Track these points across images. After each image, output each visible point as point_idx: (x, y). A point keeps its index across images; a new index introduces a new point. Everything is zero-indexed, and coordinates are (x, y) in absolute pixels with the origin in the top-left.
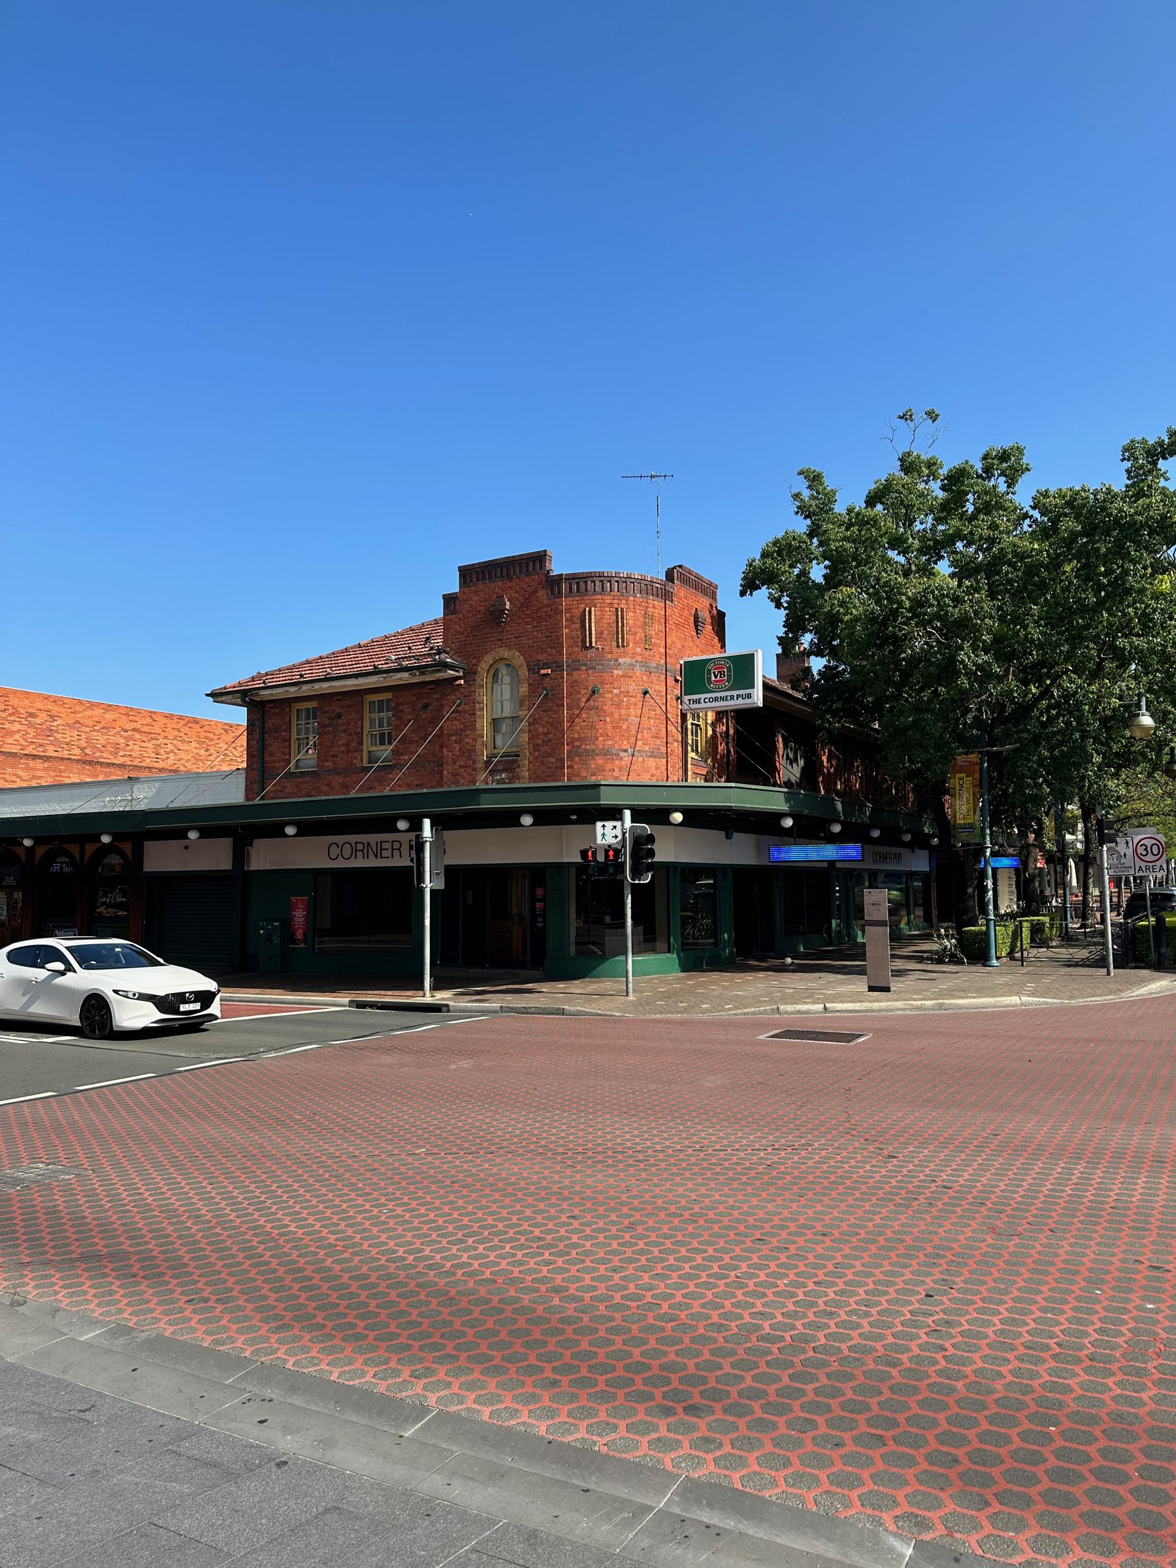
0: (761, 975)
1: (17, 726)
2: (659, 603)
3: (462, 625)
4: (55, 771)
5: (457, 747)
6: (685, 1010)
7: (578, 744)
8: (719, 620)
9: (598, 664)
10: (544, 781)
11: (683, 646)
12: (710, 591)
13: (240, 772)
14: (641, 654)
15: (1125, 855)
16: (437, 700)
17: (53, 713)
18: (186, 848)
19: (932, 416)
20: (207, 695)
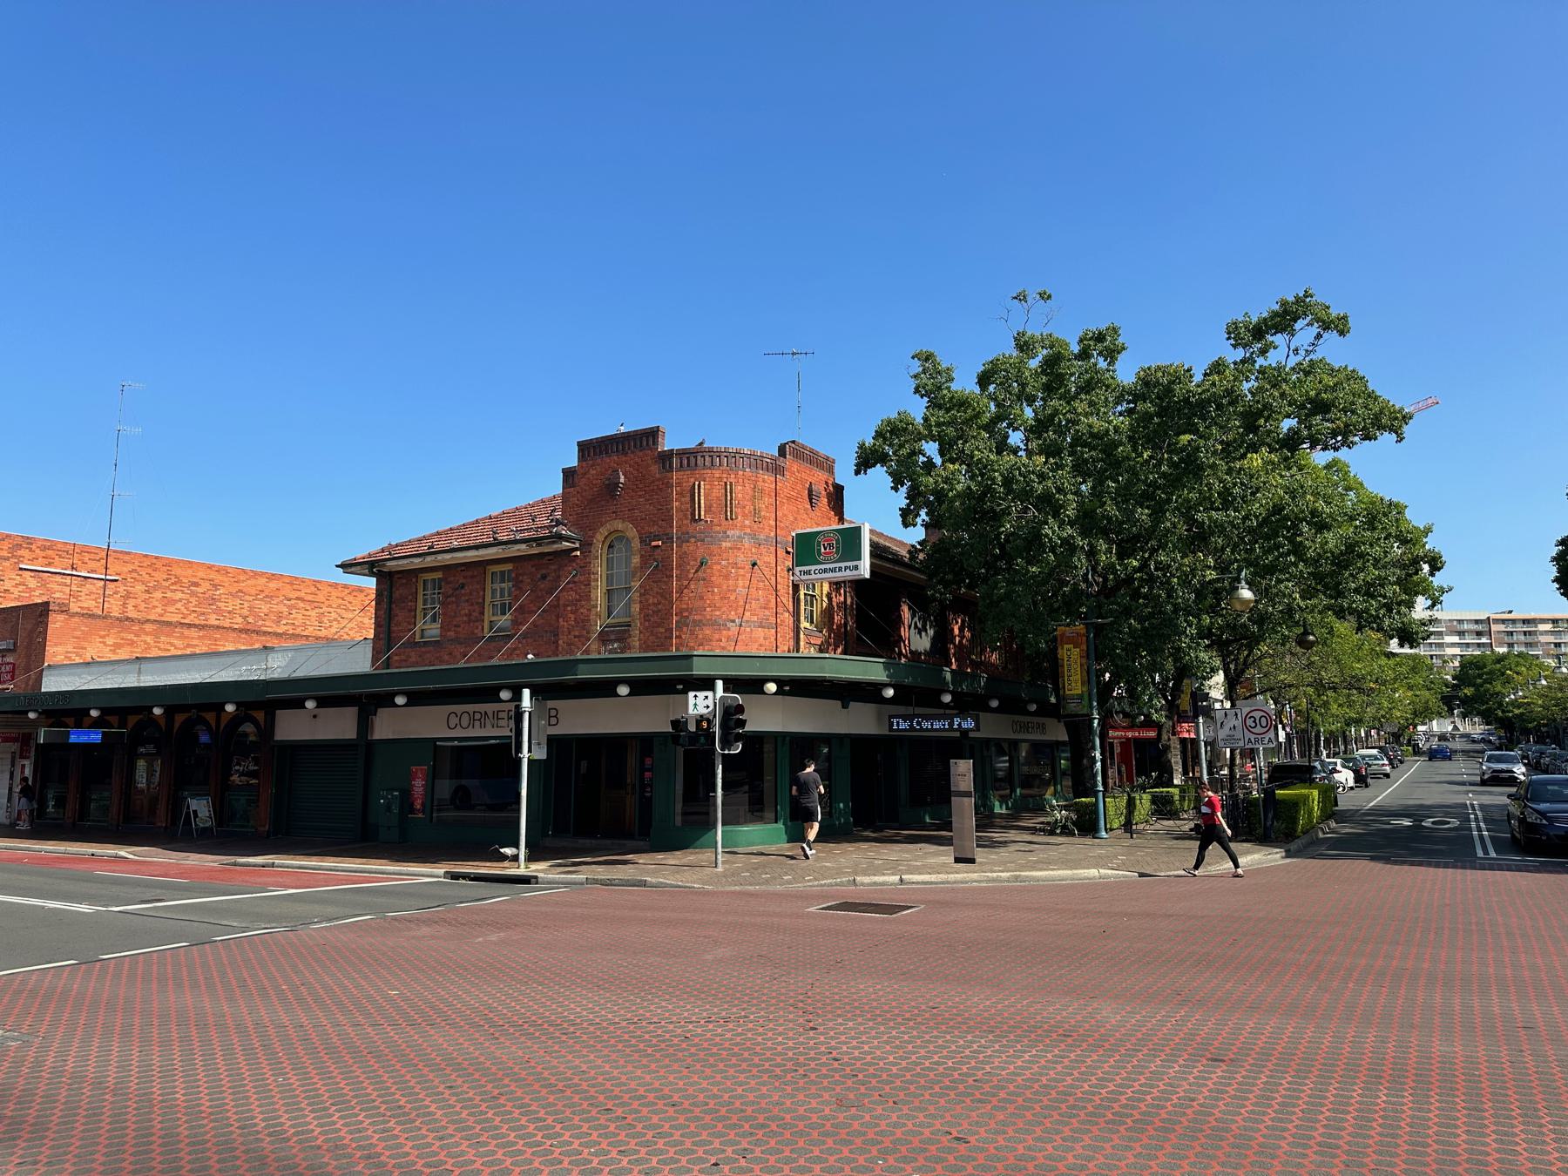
0: (865, 846)
1: (179, 595)
2: (769, 477)
5: (573, 616)
6: (767, 882)
7: (686, 614)
8: (836, 497)
10: (655, 651)
11: (796, 519)
12: (827, 465)
13: (368, 641)
14: (750, 527)
15: (1234, 727)
16: (555, 570)
17: (216, 582)
18: (315, 716)
19: (1045, 297)
20: (337, 566)
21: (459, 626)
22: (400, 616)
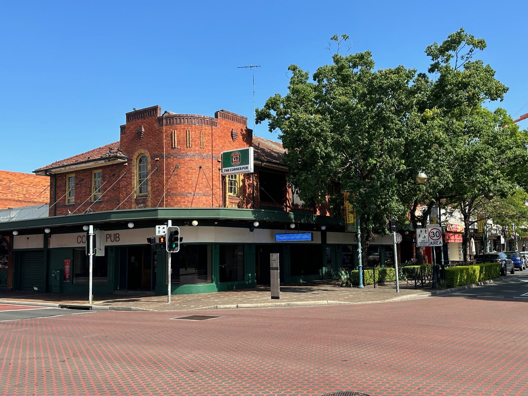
2: (208, 128)
3: (127, 139)
4: (3, 205)
7: (169, 190)
9: (178, 155)
11: (224, 146)
12: (244, 121)
14: (198, 150)
15: (425, 237)
17: (11, 179)
18: (28, 238)
19: (345, 37)
21: (82, 198)
22: (59, 193)
